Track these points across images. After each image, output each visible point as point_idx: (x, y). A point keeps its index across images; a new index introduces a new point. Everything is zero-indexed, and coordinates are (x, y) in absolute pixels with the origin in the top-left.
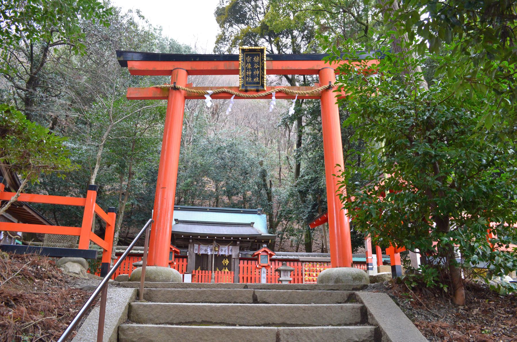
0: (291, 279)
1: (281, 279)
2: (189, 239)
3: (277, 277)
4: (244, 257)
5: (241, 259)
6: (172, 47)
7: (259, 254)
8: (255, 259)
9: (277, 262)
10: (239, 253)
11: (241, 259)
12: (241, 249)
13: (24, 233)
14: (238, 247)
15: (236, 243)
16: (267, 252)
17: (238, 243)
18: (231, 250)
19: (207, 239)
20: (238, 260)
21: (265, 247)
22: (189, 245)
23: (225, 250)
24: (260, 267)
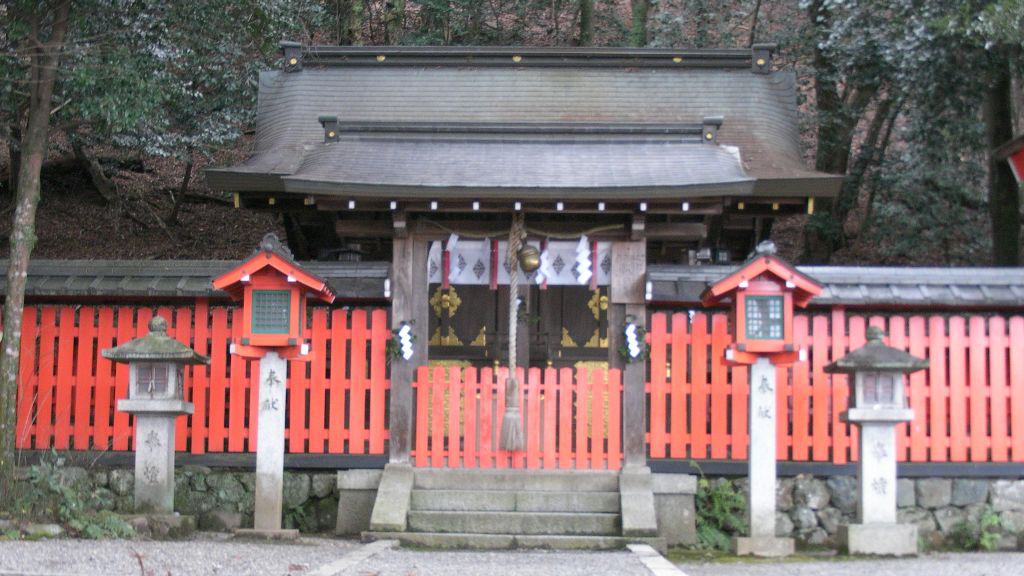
0: (909, 415)
1: (853, 415)
2: (389, 216)
3: (841, 404)
4: (670, 294)
5: (654, 307)
6: (1010, 558)
7: (737, 289)
8: (723, 305)
9: (838, 318)
10: (645, 279)
11: (654, 307)
12: (661, 253)
13: (780, 206)
14: (640, 249)
15: (629, 228)
16: (781, 281)
17: (638, 227)
18: (607, 265)
19: (477, 214)
20: (642, 314)
21: (766, 255)
22: (397, 246)
23: (570, 263)
24: (743, 358)
